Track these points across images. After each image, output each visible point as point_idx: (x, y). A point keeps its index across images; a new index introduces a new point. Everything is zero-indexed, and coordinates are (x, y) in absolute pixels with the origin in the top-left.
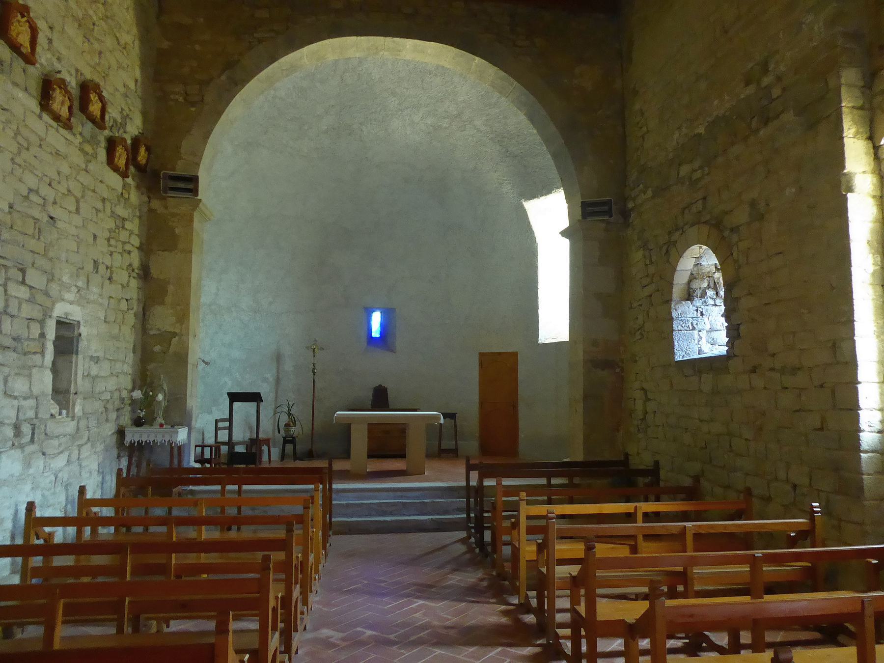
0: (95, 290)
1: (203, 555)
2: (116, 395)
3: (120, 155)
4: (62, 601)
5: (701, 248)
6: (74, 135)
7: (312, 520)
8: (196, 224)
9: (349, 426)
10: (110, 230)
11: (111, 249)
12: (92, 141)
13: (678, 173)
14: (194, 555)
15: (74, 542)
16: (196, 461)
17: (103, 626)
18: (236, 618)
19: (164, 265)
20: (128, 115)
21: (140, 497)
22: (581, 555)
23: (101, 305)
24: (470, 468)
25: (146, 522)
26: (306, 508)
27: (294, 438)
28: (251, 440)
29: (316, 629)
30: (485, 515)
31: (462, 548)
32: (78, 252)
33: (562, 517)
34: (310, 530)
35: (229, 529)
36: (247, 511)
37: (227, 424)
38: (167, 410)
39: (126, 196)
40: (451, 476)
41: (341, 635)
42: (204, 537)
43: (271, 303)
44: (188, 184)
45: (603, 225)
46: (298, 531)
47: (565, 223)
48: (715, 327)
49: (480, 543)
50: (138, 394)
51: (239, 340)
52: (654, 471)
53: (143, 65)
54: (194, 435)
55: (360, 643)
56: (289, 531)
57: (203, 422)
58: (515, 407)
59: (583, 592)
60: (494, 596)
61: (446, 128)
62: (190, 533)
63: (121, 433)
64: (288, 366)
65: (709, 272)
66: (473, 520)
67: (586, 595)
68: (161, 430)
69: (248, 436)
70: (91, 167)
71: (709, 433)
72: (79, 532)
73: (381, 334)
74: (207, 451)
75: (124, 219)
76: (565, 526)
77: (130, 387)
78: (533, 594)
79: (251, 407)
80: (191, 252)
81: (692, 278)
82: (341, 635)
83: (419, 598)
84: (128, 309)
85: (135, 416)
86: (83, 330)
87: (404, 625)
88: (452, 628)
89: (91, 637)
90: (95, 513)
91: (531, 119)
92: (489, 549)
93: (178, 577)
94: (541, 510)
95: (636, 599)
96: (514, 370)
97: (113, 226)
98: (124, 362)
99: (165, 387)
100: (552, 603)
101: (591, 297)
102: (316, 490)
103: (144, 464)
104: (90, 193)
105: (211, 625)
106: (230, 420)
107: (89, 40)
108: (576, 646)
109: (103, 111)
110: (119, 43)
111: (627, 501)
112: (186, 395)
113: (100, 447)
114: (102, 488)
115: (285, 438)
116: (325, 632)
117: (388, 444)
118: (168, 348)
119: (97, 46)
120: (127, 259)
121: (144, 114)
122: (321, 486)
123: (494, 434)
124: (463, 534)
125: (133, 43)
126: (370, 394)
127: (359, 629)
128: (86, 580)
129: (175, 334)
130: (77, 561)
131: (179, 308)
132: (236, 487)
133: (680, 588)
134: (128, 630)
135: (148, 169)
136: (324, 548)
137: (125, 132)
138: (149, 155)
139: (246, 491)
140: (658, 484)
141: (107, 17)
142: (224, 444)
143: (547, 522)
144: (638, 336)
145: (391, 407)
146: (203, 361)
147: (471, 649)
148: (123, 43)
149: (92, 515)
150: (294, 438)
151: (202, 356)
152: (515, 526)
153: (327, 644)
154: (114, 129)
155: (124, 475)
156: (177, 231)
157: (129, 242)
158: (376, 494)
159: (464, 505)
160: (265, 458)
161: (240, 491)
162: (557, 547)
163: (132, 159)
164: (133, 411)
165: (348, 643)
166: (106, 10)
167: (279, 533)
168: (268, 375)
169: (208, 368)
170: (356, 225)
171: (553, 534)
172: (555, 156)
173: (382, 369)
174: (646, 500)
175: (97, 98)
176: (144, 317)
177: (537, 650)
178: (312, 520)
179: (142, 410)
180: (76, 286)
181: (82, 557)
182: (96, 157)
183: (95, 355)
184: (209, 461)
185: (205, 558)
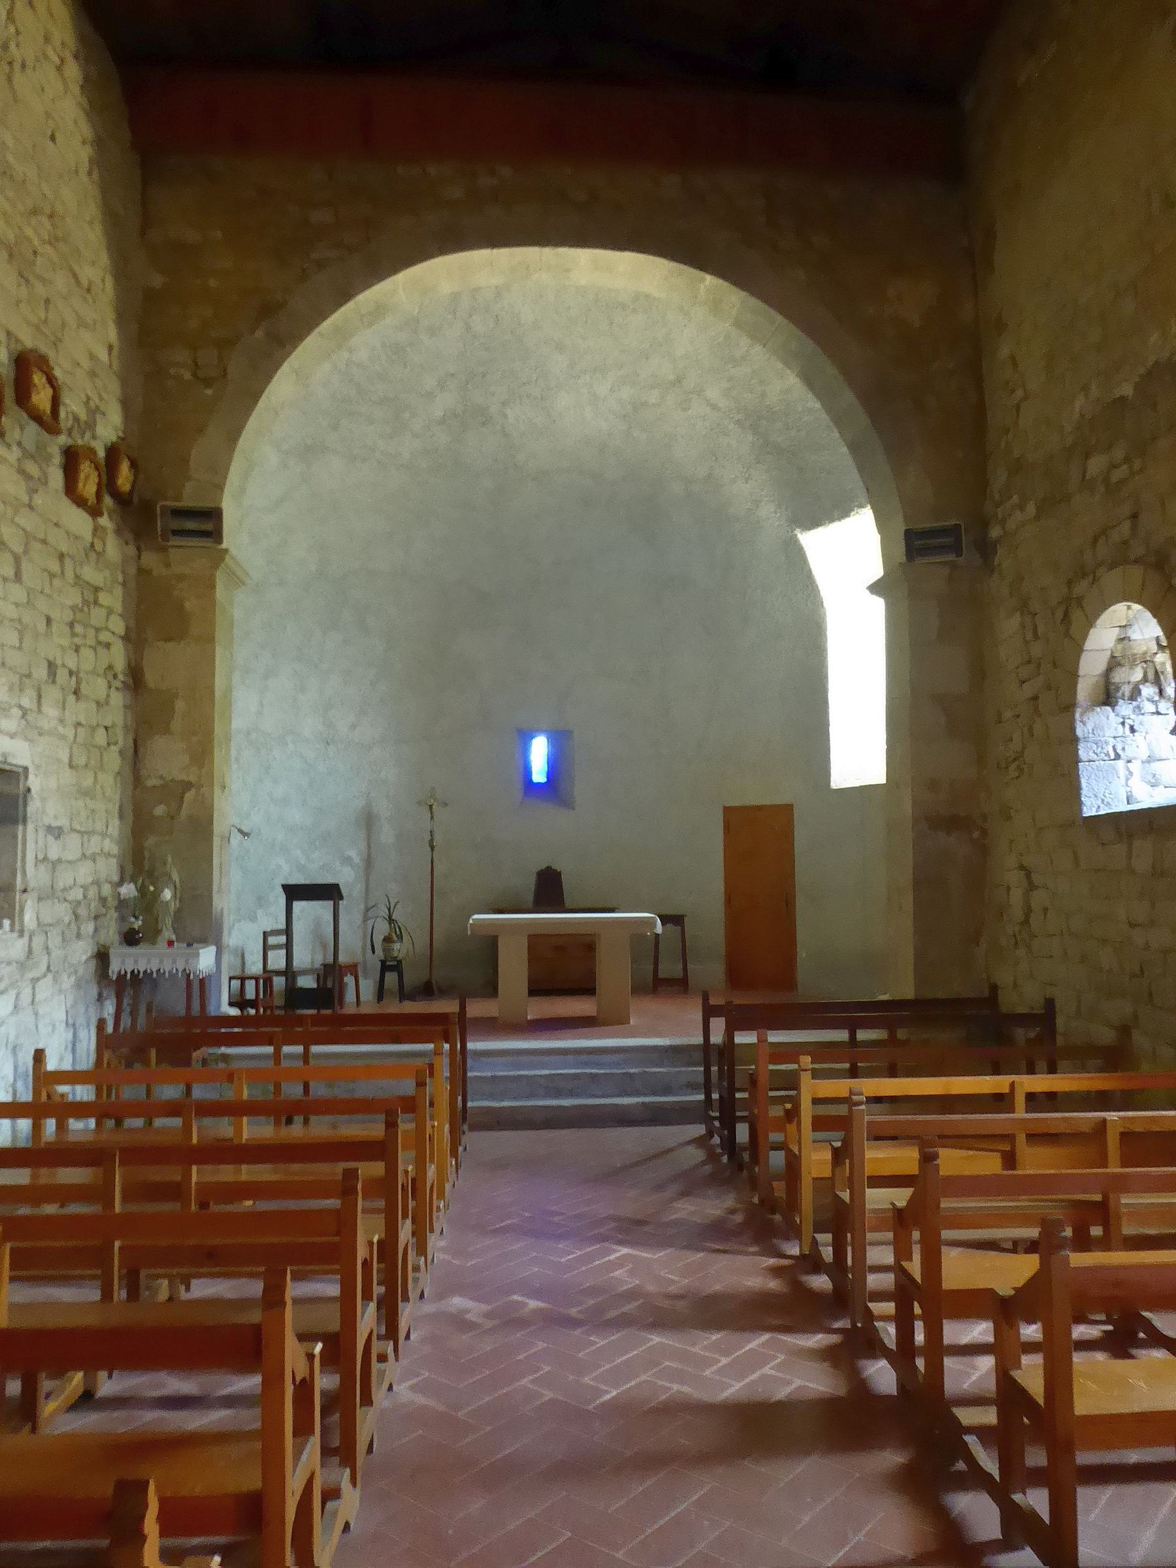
0: (51, 711)
1: (244, 1167)
2: (92, 893)
3: (87, 478)
4: (8, 1246)
5: (1129, 608)
6: (9, 446)
7: (432, 1104)
8: (220, 593)
10: (74, 608)
11: (77, 640)
12: (39, 455)
13: (1085, 472)
14: (230, 1167)
15: (30, 1145)
16: (231, 1004)
17: (80, 1287)
18: (298, 1277)
19: (167, 665)
20: (98, 408)
21: (138, 1066)
22: (913, 1168)
23: (63, 737)
24: (709, 1012)
25: (149, 1109)
26: (421, 1084)
27: (400, 962)
28: (325, 966)
29: (440, 1296)
30: (738, 1095)
31: (698, 1155)
32: (20, 648)
33: (878, 1100)
34: (428, 1123)
35: (289, 1121)
36: (319, 1090)
37: (282, 939)
38: (178, 915)
39: (98, 547)
40: (676, 1026)
41: (484, 1307)
42: (245, 1136)
43: (353, 727)
44: (205, 523)
45: (946, 571)
46: (405, 1125)
47: (876, 570)
48: (1158, 753)
49: (730, 1144)
50: (128, 890)
51: (298, 790)
52: (1046, 1016)
53: (121, 320)
54: (226, 959)
55: (520, 1323)
56: (391, 1125)
57: (244, 935)
58: (789, 903)
59: (916, 1235)
60: (756, 1240)
62: (223, 1128)
63: (102, 957)
64: (386, 835)
65: (1145, 653)
66: (716, 1105)
67: (921, 1242)
68: (169, 950)
69: (319, 960)
70: (38, 500)
71: (1147, 947)
72: (37, 1128)
74: (250, 986)
75: (97, 589)
76: (882, 1117)
77: (116, 878)
78: (825, 1238)
79: (321, 910)
81: (1114, 663)
82: (484, 1307)
83: (621, 1243)
84: (109, 744)
85: (126, 929)
86: (34, 782)
87: (593, 1291)
88: (681, 1297)
89: (56, 1305)
90: (62, 1096)
91: (809, 380)
92: (746, 1156)
93: (204, 1205)
94: (839, 1087)
95: (1014, 1251)
96: (787, 834)
97: (78, 601)
98: (104, 835)
99: (175, 876)
100: (860, 1255)
101: (923, 708)
102: (437, 1052)
103: (143, 1010)
104: (38, 546)
105: (255, 1288)
106: (288, 931)
107: (27, 281)
108: (906, 1333)
109: (56, 402)
110: (78, 282)
111: (996, 1071)
113: (68, 982)
114: (74, 1051)
115: (383, 962)
116: (457, 1302)
117: (564, 970)
118: (180, 807)
119: (41, 290)
120: (104, 658)
121: (125, 404)
122: (447, 1046)
123: (753, 955)
124: (699, 1130)
125: (103, 281)
126: (532, 881)
127: (515, 1297)
128: (50, 1209)
129: (188, 786)
130: (34, 1177)
131: (194, 739)
132: (299, 1049)
133: (1096, 1231)
134: (120, 1294)
135: (136, 499)
136: (454, 1153)
137: (94, 437)
138: (136, 476)
139: (319, 1056)
140: (1054, 1039)
141: (57, 239)
142: (278, 973)
143: (850, 1110)
144: (1012, 771)
145: (568, 903)
146: (240, 831)
147: (715, 1337)
148: (85, 284)
149: (57, 1099)
150: (400, 962)
151: (235, 820)
152: (792, 1115)
153: (460, 1322)
154: (75, 433)
155: (110, 1029)
156: (187, 605)
157: (107, 629)
158: (546, 1059)
159: (701, 1079)
160: (350, 996)
161: (306, 1056)
162: (869, 1154)
163: (108, 483)
164: (122, 919)
165: (496, 1322)
166: (54, 226)
167: (372, 1129)
169: (247, 842)
170: (497, 583)
171: (861, 1131)
172: (855, 448)
173: (549, 838)
174: (1031, 1071)
175: (44, 380)
176: (136, 755)
177: (835, 1339)
178: (432, 1104)
179: (136, 918)
180: (20, 707)
181: (44, 1171)
182: (46, 483)
183: (55, 824)
184: (253, 1004)
185: (247, 1173)
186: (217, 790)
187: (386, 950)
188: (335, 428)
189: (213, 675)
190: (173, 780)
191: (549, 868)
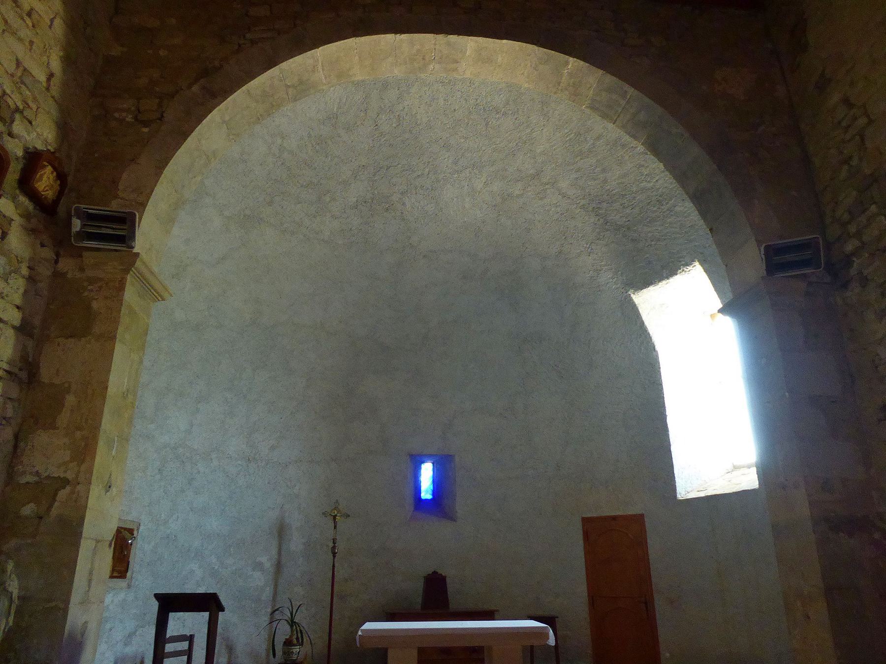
9: (385, 651)
19: (62, 361)
37: (169, 648)
43: (273, 448)
44: (118, 230)
47: (717, 303)
58: (648, 603)
61: (518, 196)
64: (296, 543)
73: (433, 494)
80: (113, 338)
96: (640, 543)
112: (67, 602)
125: (52, 21)
126: (420, 585)
129: (65, 482)
131: (78, 434)
145: (453, 606)
156: (95, 305)
168: (264, 559)
186: (95, 491)
187: (287, 653)
188: (270, 203)
189: (109, 371)
190: (48, 477)
191: (435, 573)
